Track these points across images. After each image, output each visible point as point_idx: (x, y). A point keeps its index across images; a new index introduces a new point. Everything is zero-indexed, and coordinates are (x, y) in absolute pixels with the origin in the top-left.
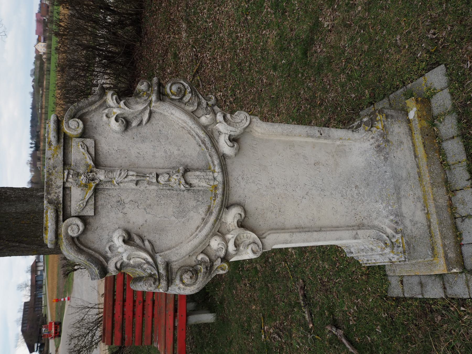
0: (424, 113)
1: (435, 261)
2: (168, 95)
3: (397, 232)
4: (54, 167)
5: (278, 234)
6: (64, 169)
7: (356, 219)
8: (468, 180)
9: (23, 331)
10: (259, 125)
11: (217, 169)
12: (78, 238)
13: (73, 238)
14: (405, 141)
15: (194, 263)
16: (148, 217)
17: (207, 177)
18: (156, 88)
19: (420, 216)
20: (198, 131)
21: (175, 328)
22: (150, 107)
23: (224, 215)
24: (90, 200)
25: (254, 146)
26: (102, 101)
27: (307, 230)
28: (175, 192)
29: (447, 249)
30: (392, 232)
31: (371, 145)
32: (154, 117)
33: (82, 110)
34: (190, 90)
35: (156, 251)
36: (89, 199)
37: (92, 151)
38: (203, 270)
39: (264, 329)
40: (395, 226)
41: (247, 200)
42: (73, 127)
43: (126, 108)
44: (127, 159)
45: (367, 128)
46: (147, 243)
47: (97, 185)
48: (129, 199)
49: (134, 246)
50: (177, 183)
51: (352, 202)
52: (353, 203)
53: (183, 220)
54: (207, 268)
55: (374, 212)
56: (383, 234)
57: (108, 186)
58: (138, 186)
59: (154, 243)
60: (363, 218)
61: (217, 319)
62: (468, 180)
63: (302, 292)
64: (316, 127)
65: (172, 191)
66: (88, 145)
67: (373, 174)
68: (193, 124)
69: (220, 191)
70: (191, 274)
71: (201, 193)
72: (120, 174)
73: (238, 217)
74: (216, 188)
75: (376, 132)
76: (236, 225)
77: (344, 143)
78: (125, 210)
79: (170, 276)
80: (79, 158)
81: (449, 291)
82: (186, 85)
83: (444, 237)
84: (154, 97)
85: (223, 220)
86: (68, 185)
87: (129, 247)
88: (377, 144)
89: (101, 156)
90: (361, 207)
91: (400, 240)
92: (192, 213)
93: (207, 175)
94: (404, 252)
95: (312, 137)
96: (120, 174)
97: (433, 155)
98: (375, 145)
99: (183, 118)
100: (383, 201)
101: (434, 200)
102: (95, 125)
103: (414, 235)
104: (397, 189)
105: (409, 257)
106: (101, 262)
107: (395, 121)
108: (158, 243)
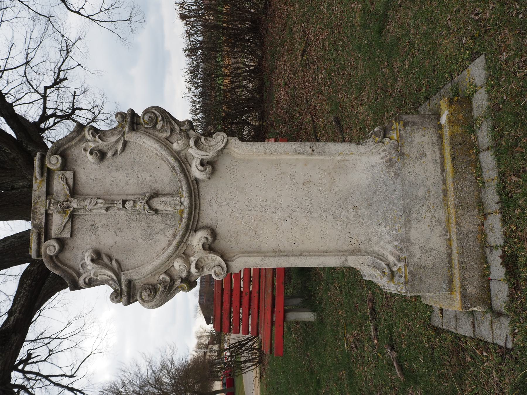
0: (461, 116)
1: (453, 296)
2: (142, 124)
3: (399, 260)
4: (39, 198)
5: (248, 258)
6: (46, 199)
7: (350, 243)
8: (497, 203)
9: (200, 303)
10: (238, 145)
11: (185, 194)
12: (57, 256)
13: (51, 257)
14: (429, 152)
15: (156, 282)
16: (118, 239)
18: (129, 120)
19: (437, 242)
21: (272, 323)
22: (124, 137)
23: (190, 238)
24: (67, 225)
26: (80, 137)
27: (284, 254)
28: (144, 216)
29: (466, 283)
30: (394, 259)
31: (382, 159)
33: (65, 145)
35: (123, 270)
36: (66, 224)
37: (71, 182)
38: (161, 289)
39: (346, 336)
40: (398, 253)
42: (53, 163)
43: (100, 141)
45: (377, 139)
46: (114, 262)
47: (73, 211)
48: (102, 223)
49: (100, 265)
50: (142, 209)
51: (347, 224)
52: (348, 226)
53: (149, 242)
54: (165, 287)
55: (374, 236)
56: (381, 262)
57: (83, 212)
58: (109, 212)
59: (121, 262)
60: (360, 242)
61: (317, 319)
62: (497, 203)
63: (371, 305)
64: (307, 143)
66: (68, 177)
67: (378, 193)
69: (185, 215)
71: (170, 217)
72: (91, 202)
73: (204, 240)
74: (182, 212)
75: (389, 144)
76: (201, 247)
77: (347, 158)
78: (98, 233)
80: (59, 189)
81: (477, 332)
82: (158, 113)
83: (463, 269)
84: (127, 128)
85: (189, 242)
86: (50, 212)
87: (96, 266)
88: (388, 157)
89: (80, 185)
90: (359, 231)
91: (403, 270)
92: (159, 236)
94: (406, 283)
95: (303, 154)
96: (91, 202)
97: (466, 169)
98: (386, 159)
99: (154, 146)
100: (386, 224)
101: (457, 224)
102: (75, 158)
103: (423, 265)
104: (407, 211)
105: (411, 289)
106: (73, 277)
107: (417, 129)
108: (125, 262)
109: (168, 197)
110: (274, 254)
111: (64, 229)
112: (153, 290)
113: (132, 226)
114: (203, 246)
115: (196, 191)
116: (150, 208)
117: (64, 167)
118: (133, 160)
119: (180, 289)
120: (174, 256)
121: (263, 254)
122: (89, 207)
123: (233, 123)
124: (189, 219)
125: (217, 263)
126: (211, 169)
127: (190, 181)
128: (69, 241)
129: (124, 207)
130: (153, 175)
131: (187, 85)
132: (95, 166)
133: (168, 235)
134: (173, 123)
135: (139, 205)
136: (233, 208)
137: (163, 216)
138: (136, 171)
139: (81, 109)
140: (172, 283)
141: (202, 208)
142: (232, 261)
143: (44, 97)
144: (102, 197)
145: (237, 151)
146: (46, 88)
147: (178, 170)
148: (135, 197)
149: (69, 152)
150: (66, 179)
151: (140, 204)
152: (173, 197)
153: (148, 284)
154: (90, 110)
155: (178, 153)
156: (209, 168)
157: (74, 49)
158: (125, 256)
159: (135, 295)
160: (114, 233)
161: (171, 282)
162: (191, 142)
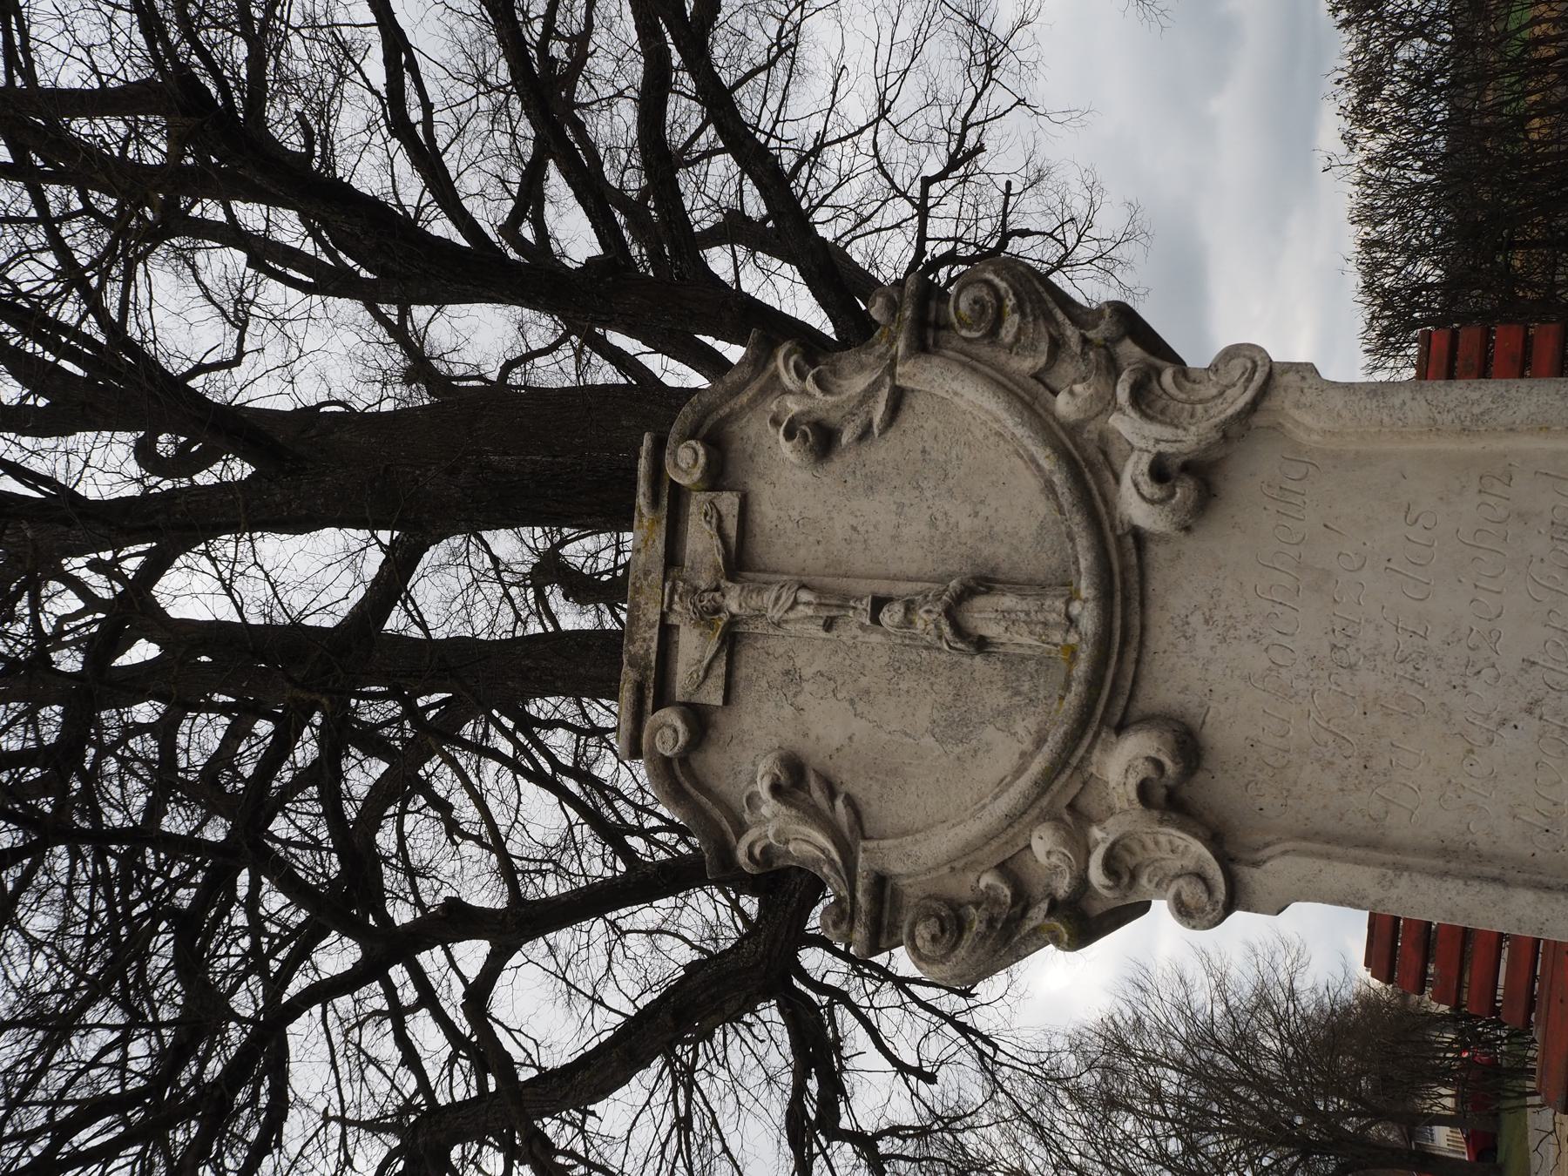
4: (647, 573)
5: (1321, 863)
6: (665, 580)
11: (1086, 588)
13: (668, 761)
15: (967, 894)
16: (858, 726)
17: (1040, 617)
18: (908, 313)
20: (1033, 449)
22: (893, 377)
23: (1096, 755)
24: (716, 664)
25: (1290, 485)
27: (1490, 870)
32: (911, 406)
33: (718, 407)
34: (1014, 301)
35: (868, 834)
41: (1213, 704)
42: (684, 466)
43: (818, 393)
44: (820, 548)
46: (839, 804)
48: (814, 669)
49: (798, 808)
50: (933, 632)
54: (991, 922)
58: (835, 633)
59: (864, 808)
65: (935, 654)
66: (723, 510)
68: (1016, 425)
69: (1081, 669)
70: (936, 930)
71: (1032, 666)
72: (778, 599)
73: (1144, 770)
74: (1072, 653)
76: (1133, 795)
79: (886, 914)
80: (700, 549)
82: (1002, 285)
86: (673, 619)
89: (759, 538)
92: (990, 733)
93: (1041, 609)
96: (778, 599)
99: (986, 405)
102: (749, 449)
106: (723, 833)
109: (1023, 596)
110: (1440, 863)
111: (706, 676)
112: (950, 921)
113: (904, 686)
114: (1144, 790)
115: (1133, 578)
116: (960, 631)
117: (717, 476)
118: (919, 456)
119: (1046, 936)
120: (1035, 812)
121: (1389, 858)
122: (775, 614)
123: (1512, 245)
124: (1094, 682)
125: (1190, 864)
126: (1193, 495)
127: (1111, 539)
128: (719, 717)
129: (875, 620)
130: (985, 511)
131: (1346, 125)
132: (804, 476)
133: (1021, 732)
134: (1060, 316)
135: (921, 619)
136: (1275, 653)
137: (1008, 660)
138: (928, 494)
139: (1024, 233)
140: (1018, 909)
141: (1152, 644)
142: (1256, 864)
143: (923, 212)
144: (816, 581)
145: (1307, 419)
146: (927, 182)
147: (1066, 498)
148: (919, 586)
149: (735, 428)
150: (720, 518)
151: (925, 616)
152: (1042, 596)
153: (937, 899)
154: (1051, 235)
155: (1073, 429)
156: (1184, 491)
157: (1008, 60)
158: (875, 787)
159: (894, 928)
160: (846, 704)
161: (1014, 903)
162: (1119, 388)
